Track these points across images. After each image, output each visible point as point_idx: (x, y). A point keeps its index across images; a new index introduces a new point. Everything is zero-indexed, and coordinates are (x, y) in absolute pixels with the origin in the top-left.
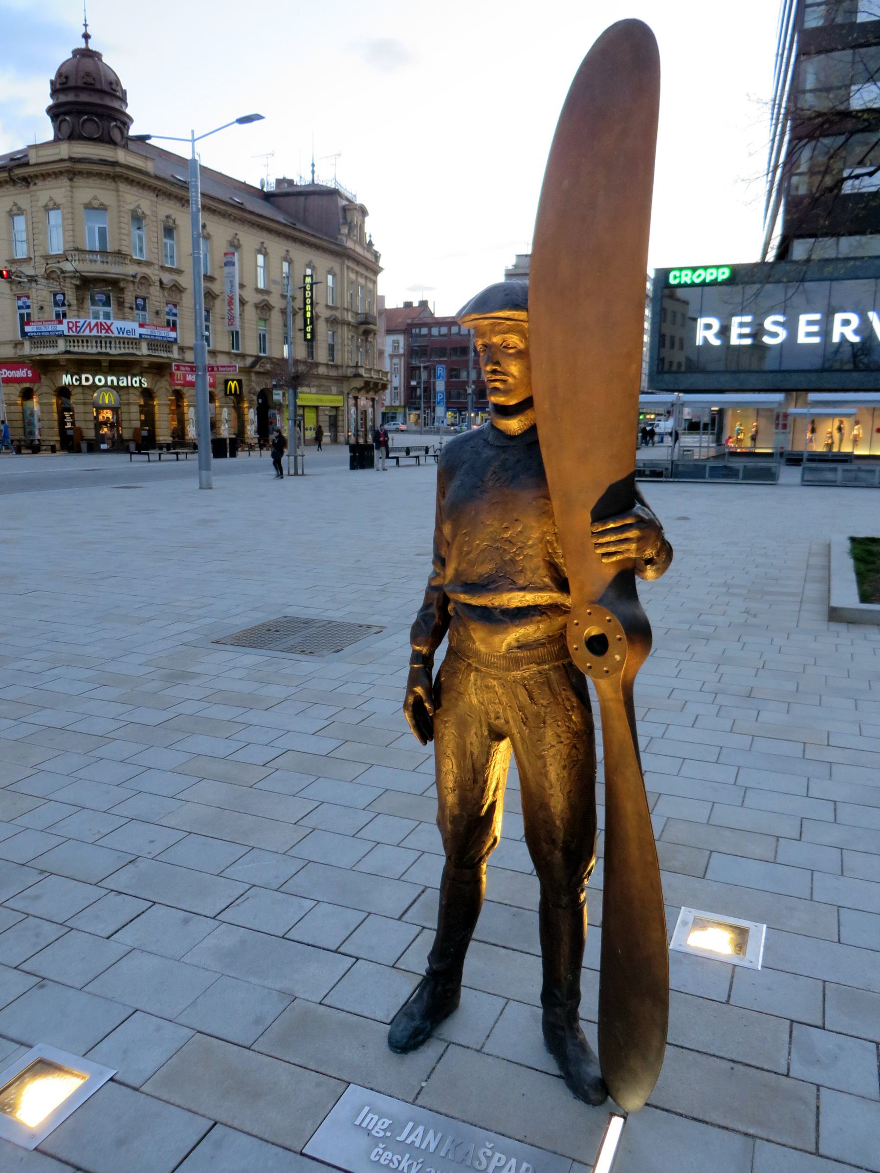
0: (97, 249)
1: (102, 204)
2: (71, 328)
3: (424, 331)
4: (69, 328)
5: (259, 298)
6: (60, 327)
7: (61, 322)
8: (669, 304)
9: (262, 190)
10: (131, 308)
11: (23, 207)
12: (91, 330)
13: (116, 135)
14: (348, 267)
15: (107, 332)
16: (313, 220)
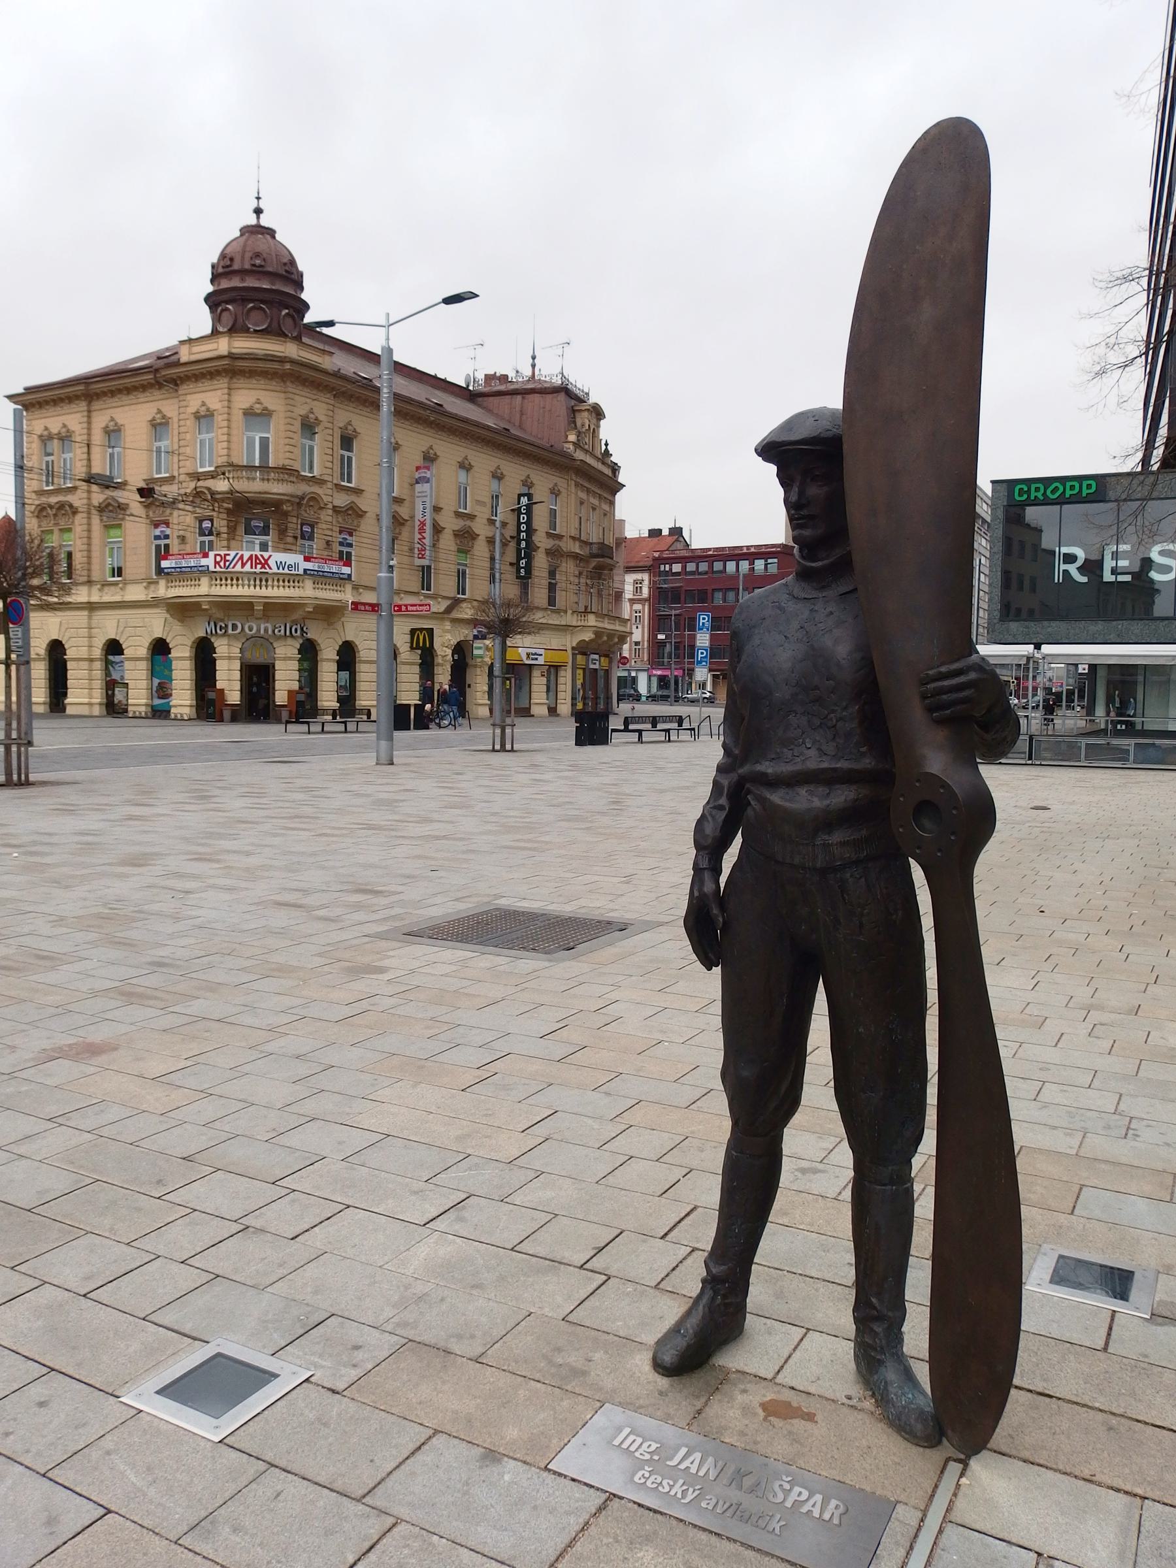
0: (257, 464)
1: (266, 409)
4: (216, 563)
6: (204, 562)
7: (206, 555)
12: (243, 565)
15: (263, 567)
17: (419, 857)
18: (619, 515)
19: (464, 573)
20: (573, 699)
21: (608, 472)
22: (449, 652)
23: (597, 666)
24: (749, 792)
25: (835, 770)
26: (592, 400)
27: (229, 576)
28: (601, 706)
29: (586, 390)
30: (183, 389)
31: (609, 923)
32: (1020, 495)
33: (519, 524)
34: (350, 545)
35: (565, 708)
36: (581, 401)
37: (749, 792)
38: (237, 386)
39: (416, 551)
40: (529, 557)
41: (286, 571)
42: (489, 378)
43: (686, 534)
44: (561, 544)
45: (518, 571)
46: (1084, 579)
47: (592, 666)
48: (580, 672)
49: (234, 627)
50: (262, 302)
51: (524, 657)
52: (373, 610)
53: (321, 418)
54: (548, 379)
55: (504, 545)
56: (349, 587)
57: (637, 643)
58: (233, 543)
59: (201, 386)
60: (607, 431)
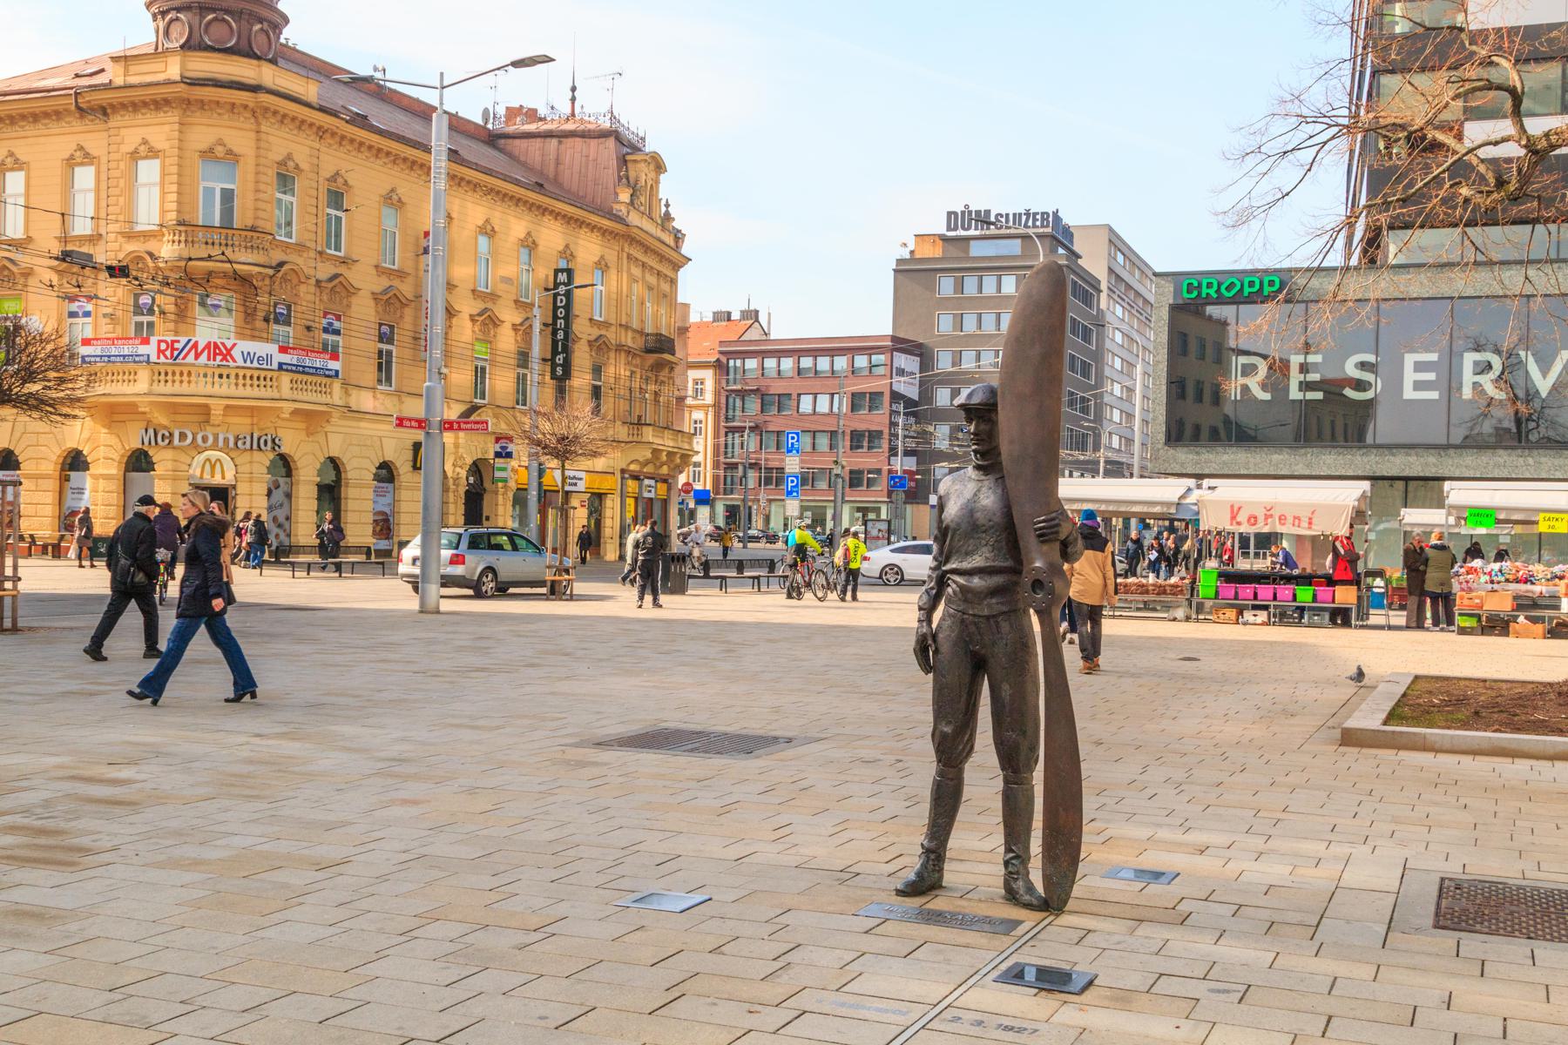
0: (217, 224)
1: (230, 152)
2: (163, 352)
3: (751, 364)
4: (159, 351)
5: (596, 332)
6: (143, 349)
7: (146, 341)
8: (1192, 325)
9: (484, 128)
10: (266, 320)
11: (94, 152)
12: (197, 356)
13: (259, 44)
14: (629, 257)
15: (224, 359)
16: (584, 178)
18: (681, 298)
19: (483, 369)
21: (670, 241)
22: (463, 474)
23: (652, 495)
27: (177, 369)
30: (116, 121)
31: (776, 738)
33: (555, 308)
34: (337, 332)
36: (636, 149)
38: (190, 120)
40: (566, 350)
41: (255, 364)
42: (512, 113)
43: (763, 319)
45: (553, 371)
46: (1267, 396)
47: (646, 495)
48: (630, 502)
49: (183, 436)
50: (227, 11)
52: (420, 427)
53: (303, 166)
56: (337, 385)
58: (182, 327)
59: (140, 118)
60: (667, 188)
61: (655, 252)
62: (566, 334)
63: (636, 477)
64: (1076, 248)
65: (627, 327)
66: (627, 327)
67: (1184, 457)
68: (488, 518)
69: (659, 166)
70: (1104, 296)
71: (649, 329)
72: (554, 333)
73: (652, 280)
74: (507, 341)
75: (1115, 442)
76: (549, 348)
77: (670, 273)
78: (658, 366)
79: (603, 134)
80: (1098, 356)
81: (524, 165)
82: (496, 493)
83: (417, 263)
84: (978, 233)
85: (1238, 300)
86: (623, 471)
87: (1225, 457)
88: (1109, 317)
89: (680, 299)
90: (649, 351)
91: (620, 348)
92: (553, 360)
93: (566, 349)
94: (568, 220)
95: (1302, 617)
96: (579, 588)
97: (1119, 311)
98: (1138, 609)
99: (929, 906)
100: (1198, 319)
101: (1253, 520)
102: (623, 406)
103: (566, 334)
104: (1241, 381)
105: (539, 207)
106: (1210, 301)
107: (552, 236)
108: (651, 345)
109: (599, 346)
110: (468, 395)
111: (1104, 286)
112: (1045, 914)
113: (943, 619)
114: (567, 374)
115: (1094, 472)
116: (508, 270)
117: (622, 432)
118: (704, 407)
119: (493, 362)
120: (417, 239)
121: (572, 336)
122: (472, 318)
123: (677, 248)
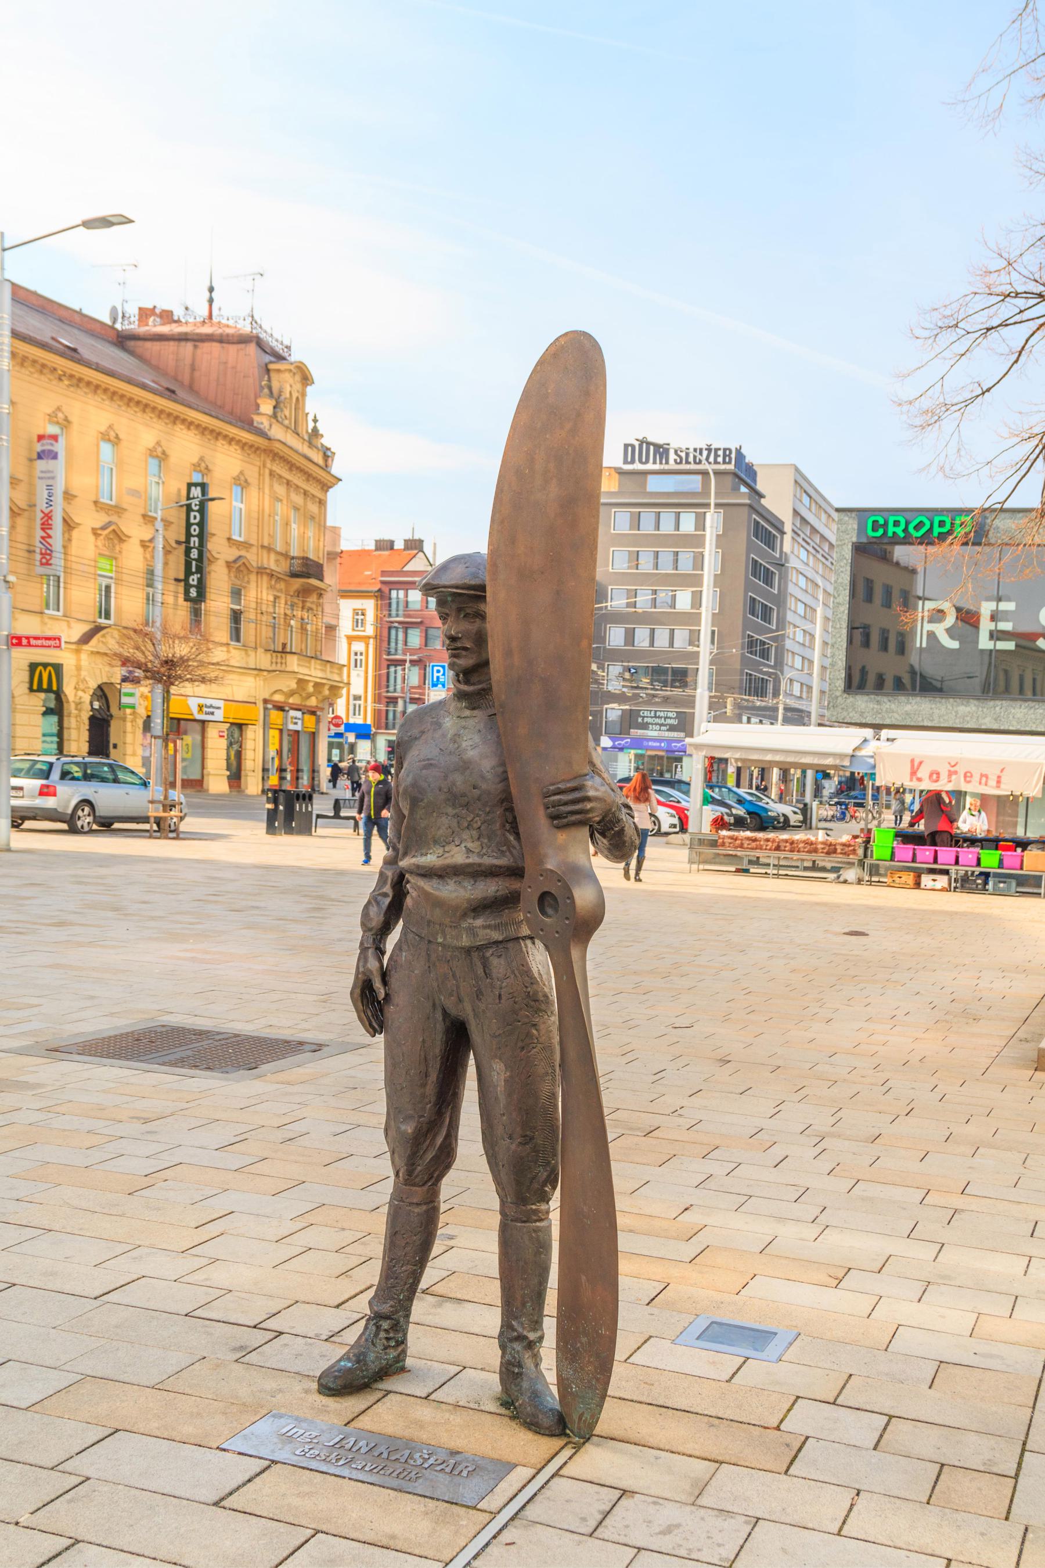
9: (113, 328)
17: (57, 966)
19: (108, 588)
20: (265, 770)
21: (318, 458)
22: (87, 698)
23: (298, 727)
24: (408, 882)
25: (480, 865)
26: (295, 357)
28: (305, 780)
29: (286, 342)
31: (301, 1043)
32: (874, 529)
33: (189, 525)
35: (253, 785)
36: (280, 358)
37: (408, 882)
39: (38, 557)
42: (145, 314)
43: (428, 548)
44: (248, 556)
45: (187, 592)
46: (954, 645)
47: (292, 727)
48: (274, 734)
51: (195, 710)
54: (231, 323)
55: (167, 552)
57: (357, 698)
60: (316, 404)
61: (300, 470)
62: (201, 554)
63: (281, 708)
64: (760, 487)
65: (269, 549)
66: (269, 549)
67: (864, 704)
68: (115, 746)
69: (306, 379)
70: (788, 538)
71: (295, 552)
72: (188, 551)
73: (298, 499)
74: (133, 558)
75: (796, 689)
76: (182, 568)
77: (319, 494)
78: (305, 592)
79: (243, 340)
80: (780, 600)
81: (156, 368)
82: (124, 719)
83: (31, 469)
84: (657, 467)
85: (927, 540)
86: (265, 701)
87: (908, 708)
88: (793, 563)
89: (329, 523)
90: (294, 575)
91: (261, 571)
92: (186, 580)
93: (200, 570)
94: (203, 430)
95: (986, 883)
96: (189, 824)
97: (803, 554)
98: (806, 869)
99: (365, 1422)
100: (881, 556)
101: (935, 776)
102: (266, 632)
103: (201, 554)
104: (928, 627)
105: (169, 415)
106: (895, 540)
107: (186, 447)
108: (297, 569)
109: (238, 567)
110: (91, 614)
111: (788, 528)
112: (557, 1443)
113: (398, 947)
114: (201, 596)
115: (773, 720)
116: (133, 482)
117: (264, 660)
118: (365, 639)
119: (118, 581)
120: (31, 442)
121: (206, 555)
122: (95, 532)
123: (326, 468)
